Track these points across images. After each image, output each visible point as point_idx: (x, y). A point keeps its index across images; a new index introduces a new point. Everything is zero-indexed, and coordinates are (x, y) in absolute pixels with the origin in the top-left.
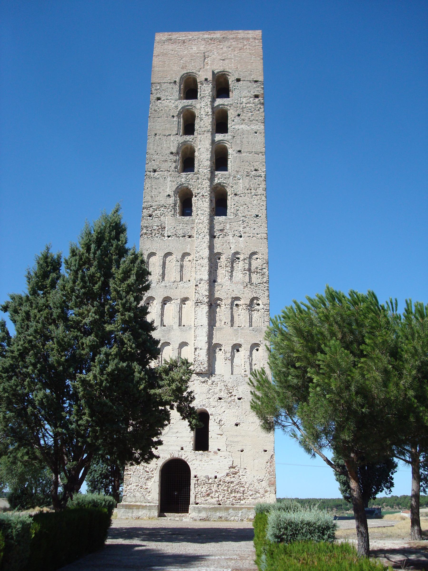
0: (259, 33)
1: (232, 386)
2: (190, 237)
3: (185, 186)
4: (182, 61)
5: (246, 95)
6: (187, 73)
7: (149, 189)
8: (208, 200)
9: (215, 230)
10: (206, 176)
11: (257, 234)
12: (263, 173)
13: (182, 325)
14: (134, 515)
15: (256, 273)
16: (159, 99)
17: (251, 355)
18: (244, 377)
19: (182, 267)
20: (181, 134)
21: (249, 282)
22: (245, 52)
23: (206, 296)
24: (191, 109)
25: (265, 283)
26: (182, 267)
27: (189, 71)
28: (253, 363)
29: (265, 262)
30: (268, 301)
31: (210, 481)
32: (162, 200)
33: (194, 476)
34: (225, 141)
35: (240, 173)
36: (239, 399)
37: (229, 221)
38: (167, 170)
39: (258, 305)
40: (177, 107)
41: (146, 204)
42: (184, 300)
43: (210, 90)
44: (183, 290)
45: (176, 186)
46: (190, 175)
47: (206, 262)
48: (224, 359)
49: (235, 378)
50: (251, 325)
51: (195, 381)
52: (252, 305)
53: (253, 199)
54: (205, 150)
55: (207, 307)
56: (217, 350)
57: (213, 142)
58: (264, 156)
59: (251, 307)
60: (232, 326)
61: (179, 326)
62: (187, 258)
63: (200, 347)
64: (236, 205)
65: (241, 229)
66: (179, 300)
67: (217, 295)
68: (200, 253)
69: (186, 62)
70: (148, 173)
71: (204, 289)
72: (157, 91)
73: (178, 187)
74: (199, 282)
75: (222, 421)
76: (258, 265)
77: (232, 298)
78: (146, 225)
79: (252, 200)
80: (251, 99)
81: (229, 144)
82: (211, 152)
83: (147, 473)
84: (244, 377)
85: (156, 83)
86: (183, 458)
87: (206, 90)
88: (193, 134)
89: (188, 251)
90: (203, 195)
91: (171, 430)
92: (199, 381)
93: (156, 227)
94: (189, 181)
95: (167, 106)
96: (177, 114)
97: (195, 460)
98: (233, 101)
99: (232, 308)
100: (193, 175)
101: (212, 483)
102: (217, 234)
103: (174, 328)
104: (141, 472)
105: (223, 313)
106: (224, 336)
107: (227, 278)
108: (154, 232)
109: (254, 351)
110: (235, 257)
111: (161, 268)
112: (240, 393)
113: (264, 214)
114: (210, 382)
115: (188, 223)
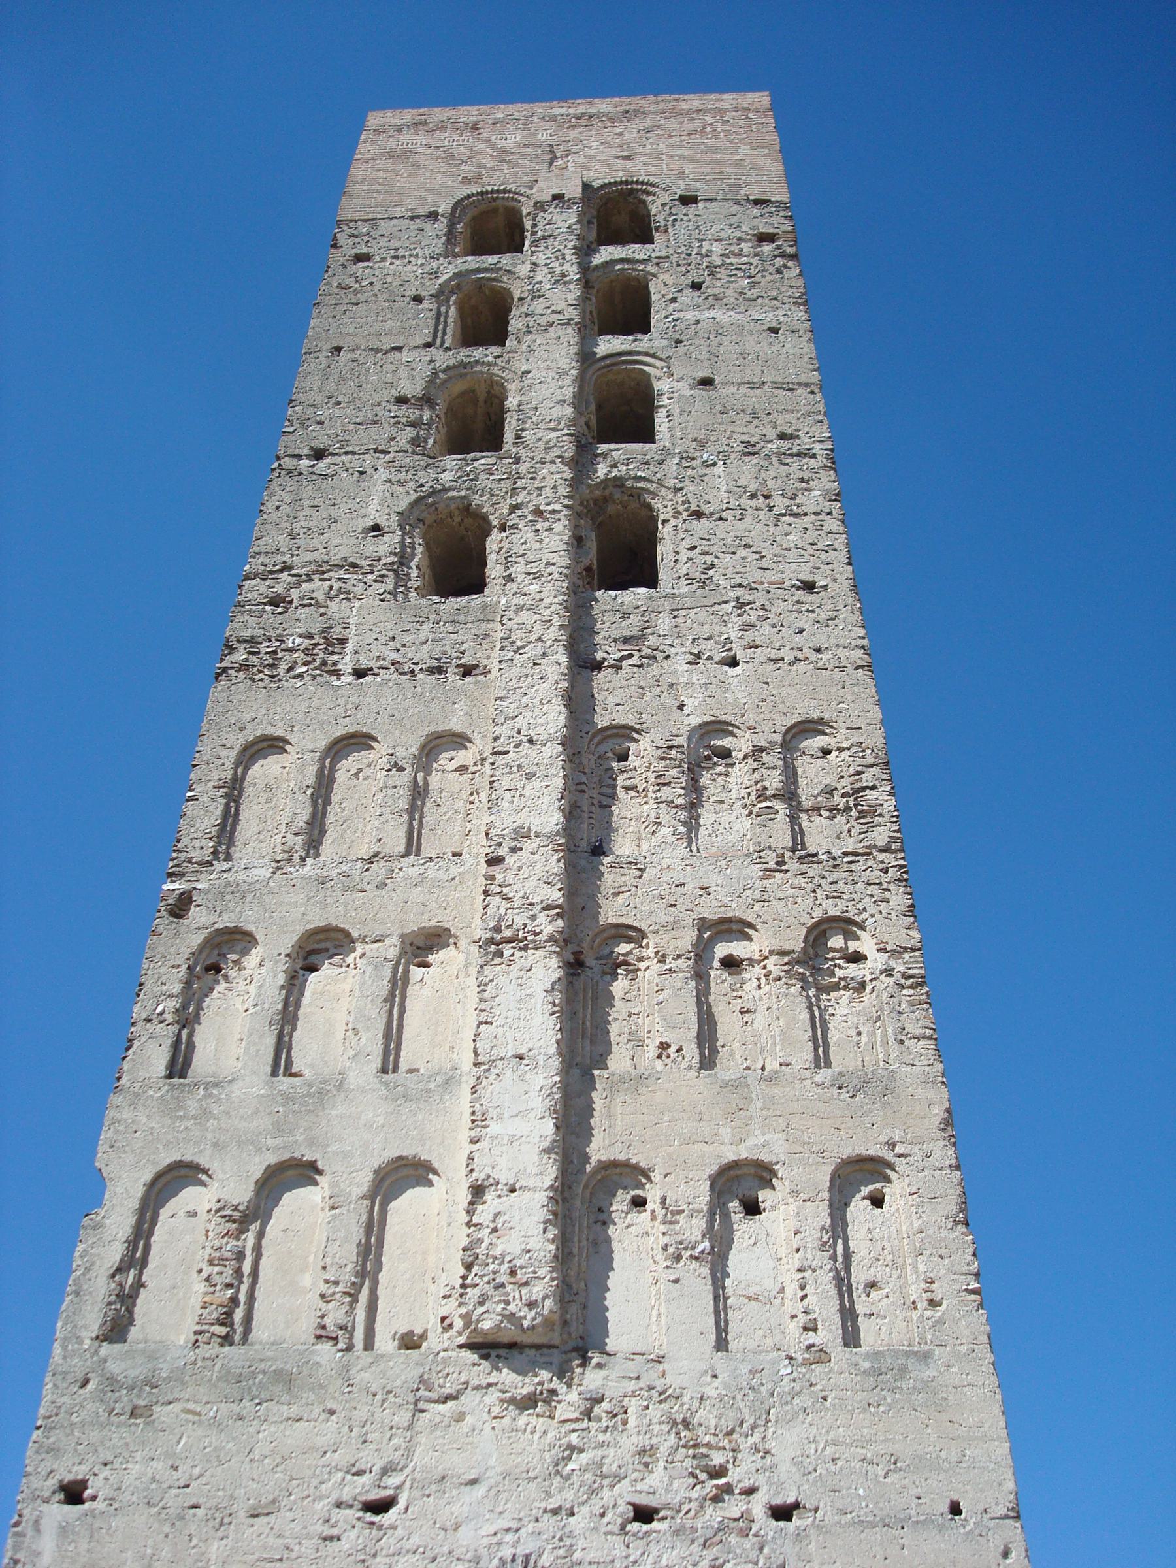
1: (728, 1422)
2: (467, 671)
3: (453, 498)
5: (723, 234)
6: (482, 193)
7: (286, 509)
9: (598, 639)
11: (818, 650)
12: (817, 446)
13: (403, 1065)
15: (825, 813)
17: (838, 1226)
18: (806, 1363)
19: (419, 793)
23: (548, 907)
24: (494, 280)
25: (886, 849)
26: (419, 793)
28: (859, 1276)
32: (342, 544)
34: (639, 353)
35: (711, 448)
36: (782, 1513)
37: (668, 604)
38: (376, 451)
39: (857, 958)
40: (435, 274)
41: (262, 559)
42: (423, 945)
44: (417, 895)
45: (414, 496)
46: (483, 461)
47: (549, 758)
48: (660, 1257)
49: (744, 1369)
50: (822, 1060)
51: (469, 1400)
52: (816, 957)
53: (783, 527)
54: (552, 374)
55: (554, 962)
56: (620, 1203)
57: (586, 357)
58: (818, 397)
59: (816, 970)
60: (708, 1062)
61: (384, 1070)
62: (448, 761)
64: (699, 550)
65: (733, 631)
66: (394, 940)
67: (612, 912)
68: (520, 723)
70: (288, 462)
71: (537, 876)
73: (419, 500)
74: (508, 844)
76: (835, 777)
77: (703, 924)
78: (249, 633)
81: (658, 363)
84: (806, 1363)
85: (356, 221)
89: (455, 724)
92: (493, 1396)
93: (298, 640)
94: (476, 479)
99: (700, 976)
100: (493, 461)
102: (608, 652)
103: (354, 1079)
105: (648, 1004)
106: (660, 1121)
107: (666, 831)
108: (289, 658)
109: (859, 1208)
110: (708, 747)
111: (305, 799)
112: (785, 1468)
113: (841, 579)
114: (570, 1400)
115: (461, 618)
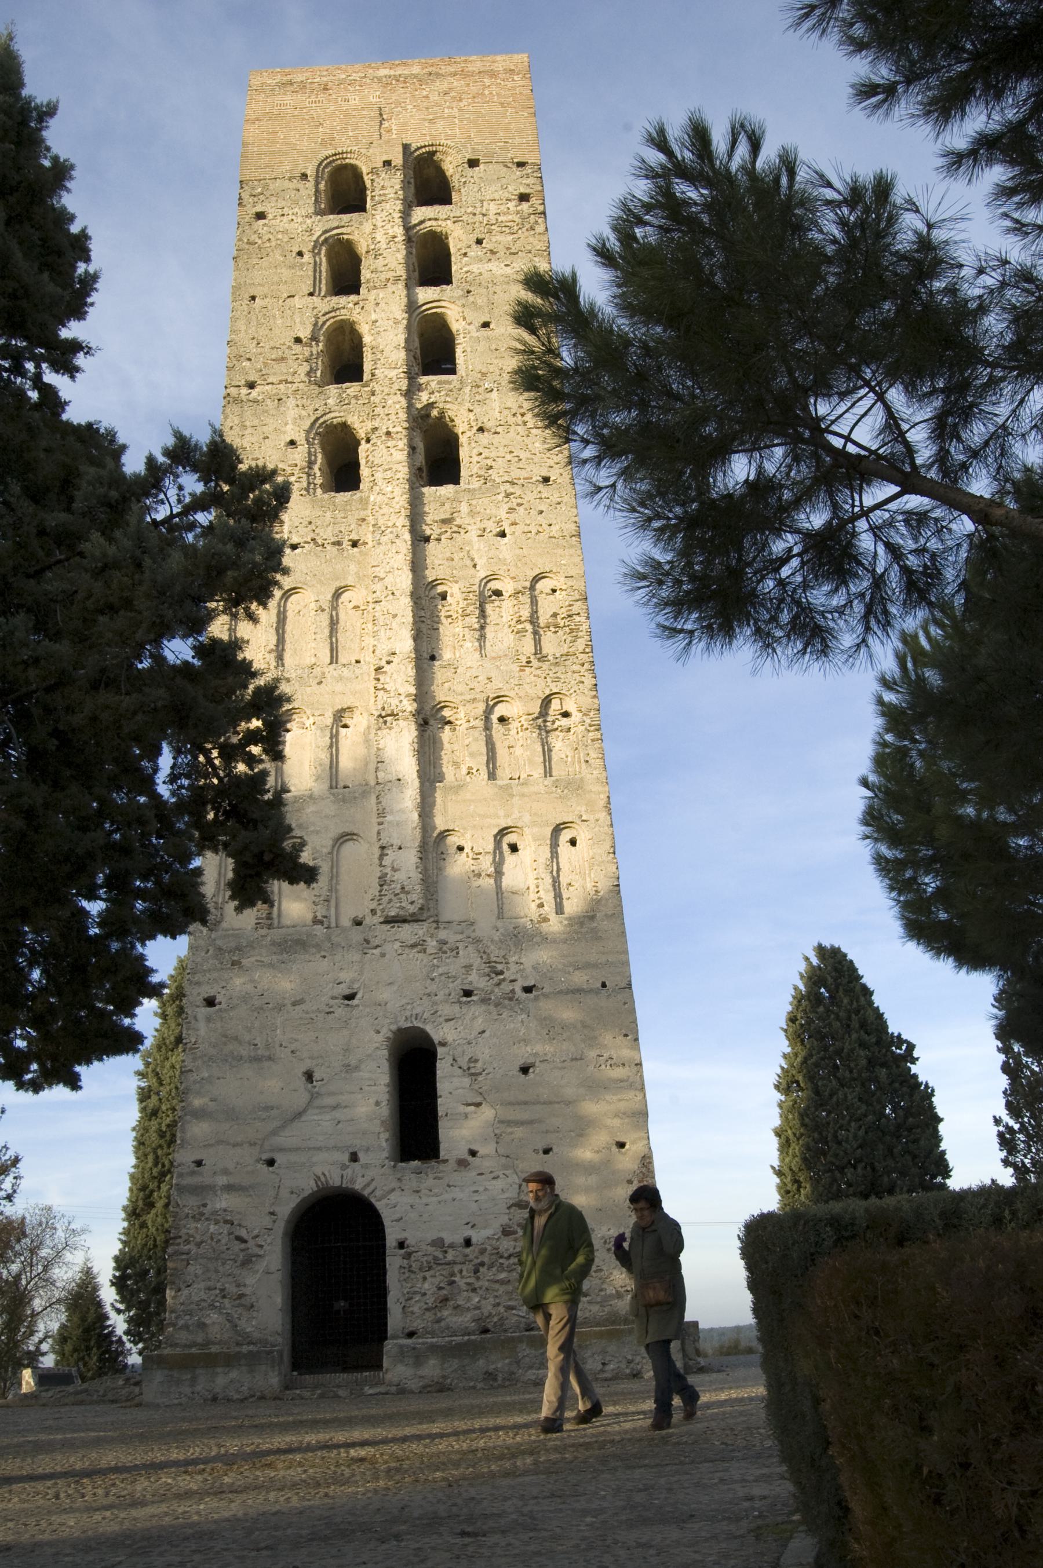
0: (521, 59)
2: (355, 544)
4: (321, 129)
8: (402, 444)
10: (396, 386)
14: (198, 1388)
16: (261, 216)
19: (334, 624)
20: (323, 294)
21: (536, 654)
22: (488, 102)
26: (334, 624)
27: (340, 150)
29: (578, 597)
30: (596, 701)
31: (450, 1257)
33: (395, 1244)
36: (528, 990)
39: (566, 715)
43: (398, 187)
44: (339, 687)
46: (352, 389)
47: (404, 606)
54: (391, 322)
55: (413, 727)
57: (412, 306)
60: (492, 776)
61: (331, 787)
63: (396, 842)
64: (483, 456)
65: (502, 513)
69: (331, 130)
71: (401, 679)
72: (256, 199)
75: (476, 1061)
79: (527, 440)
80: (511, 205)
82: (408, 328)
83: (243, 1246)
86: (358, 1187)
87: (387, 192)
88: (358, 293)
90: (388, 433)
91: (318, 1102)
92: (397, 945)
95: (285, 232)
96: (310, 247)
97: (398, 1193)
98: (463, 210)
101: (458, 1260)
104: (223, 1241)
